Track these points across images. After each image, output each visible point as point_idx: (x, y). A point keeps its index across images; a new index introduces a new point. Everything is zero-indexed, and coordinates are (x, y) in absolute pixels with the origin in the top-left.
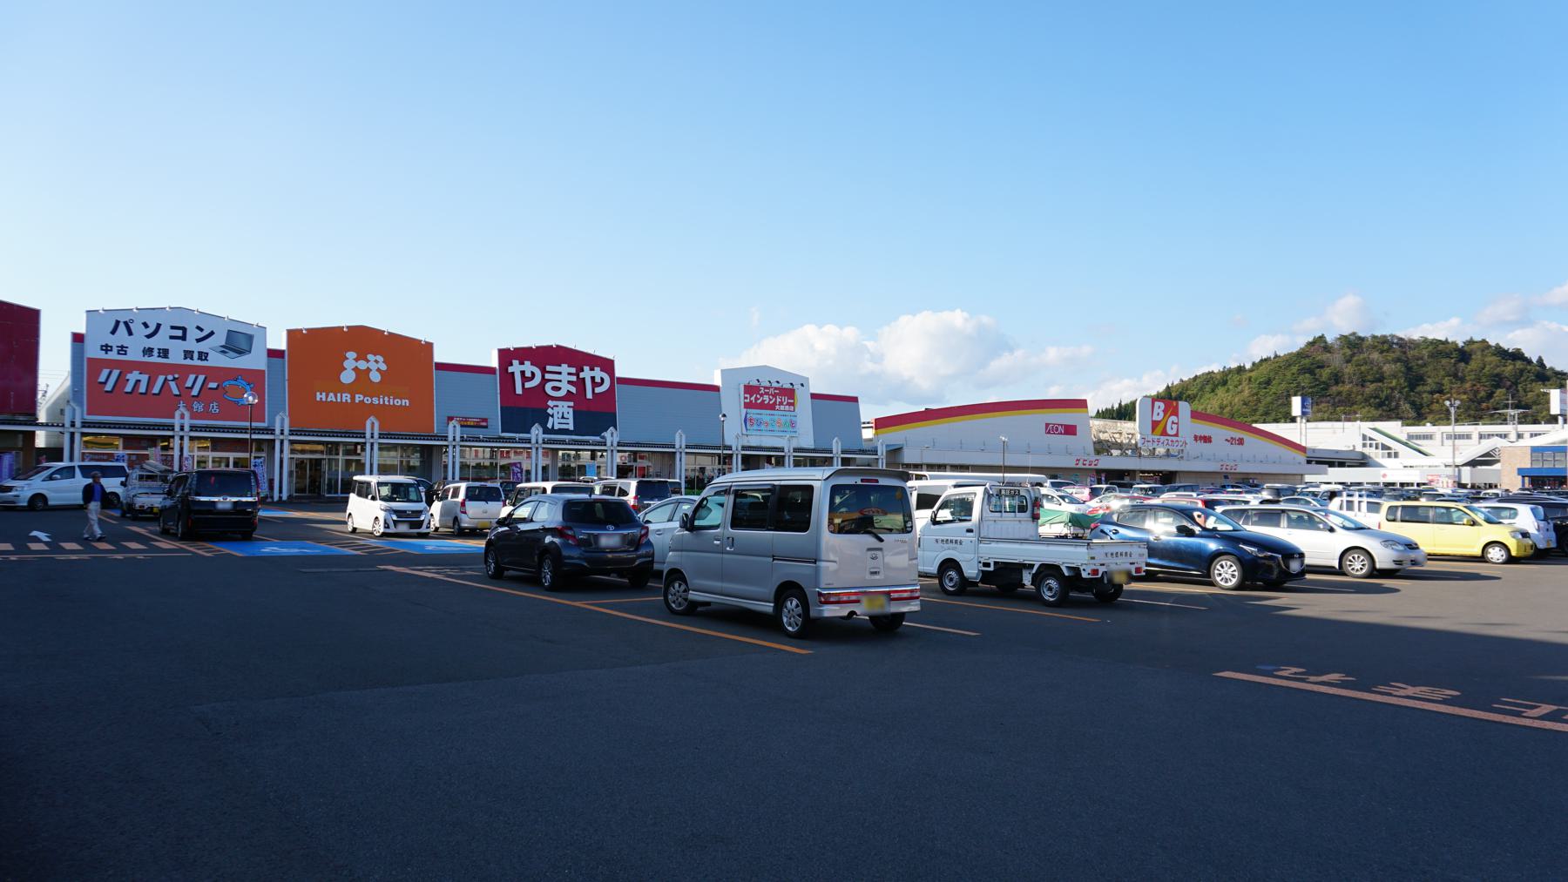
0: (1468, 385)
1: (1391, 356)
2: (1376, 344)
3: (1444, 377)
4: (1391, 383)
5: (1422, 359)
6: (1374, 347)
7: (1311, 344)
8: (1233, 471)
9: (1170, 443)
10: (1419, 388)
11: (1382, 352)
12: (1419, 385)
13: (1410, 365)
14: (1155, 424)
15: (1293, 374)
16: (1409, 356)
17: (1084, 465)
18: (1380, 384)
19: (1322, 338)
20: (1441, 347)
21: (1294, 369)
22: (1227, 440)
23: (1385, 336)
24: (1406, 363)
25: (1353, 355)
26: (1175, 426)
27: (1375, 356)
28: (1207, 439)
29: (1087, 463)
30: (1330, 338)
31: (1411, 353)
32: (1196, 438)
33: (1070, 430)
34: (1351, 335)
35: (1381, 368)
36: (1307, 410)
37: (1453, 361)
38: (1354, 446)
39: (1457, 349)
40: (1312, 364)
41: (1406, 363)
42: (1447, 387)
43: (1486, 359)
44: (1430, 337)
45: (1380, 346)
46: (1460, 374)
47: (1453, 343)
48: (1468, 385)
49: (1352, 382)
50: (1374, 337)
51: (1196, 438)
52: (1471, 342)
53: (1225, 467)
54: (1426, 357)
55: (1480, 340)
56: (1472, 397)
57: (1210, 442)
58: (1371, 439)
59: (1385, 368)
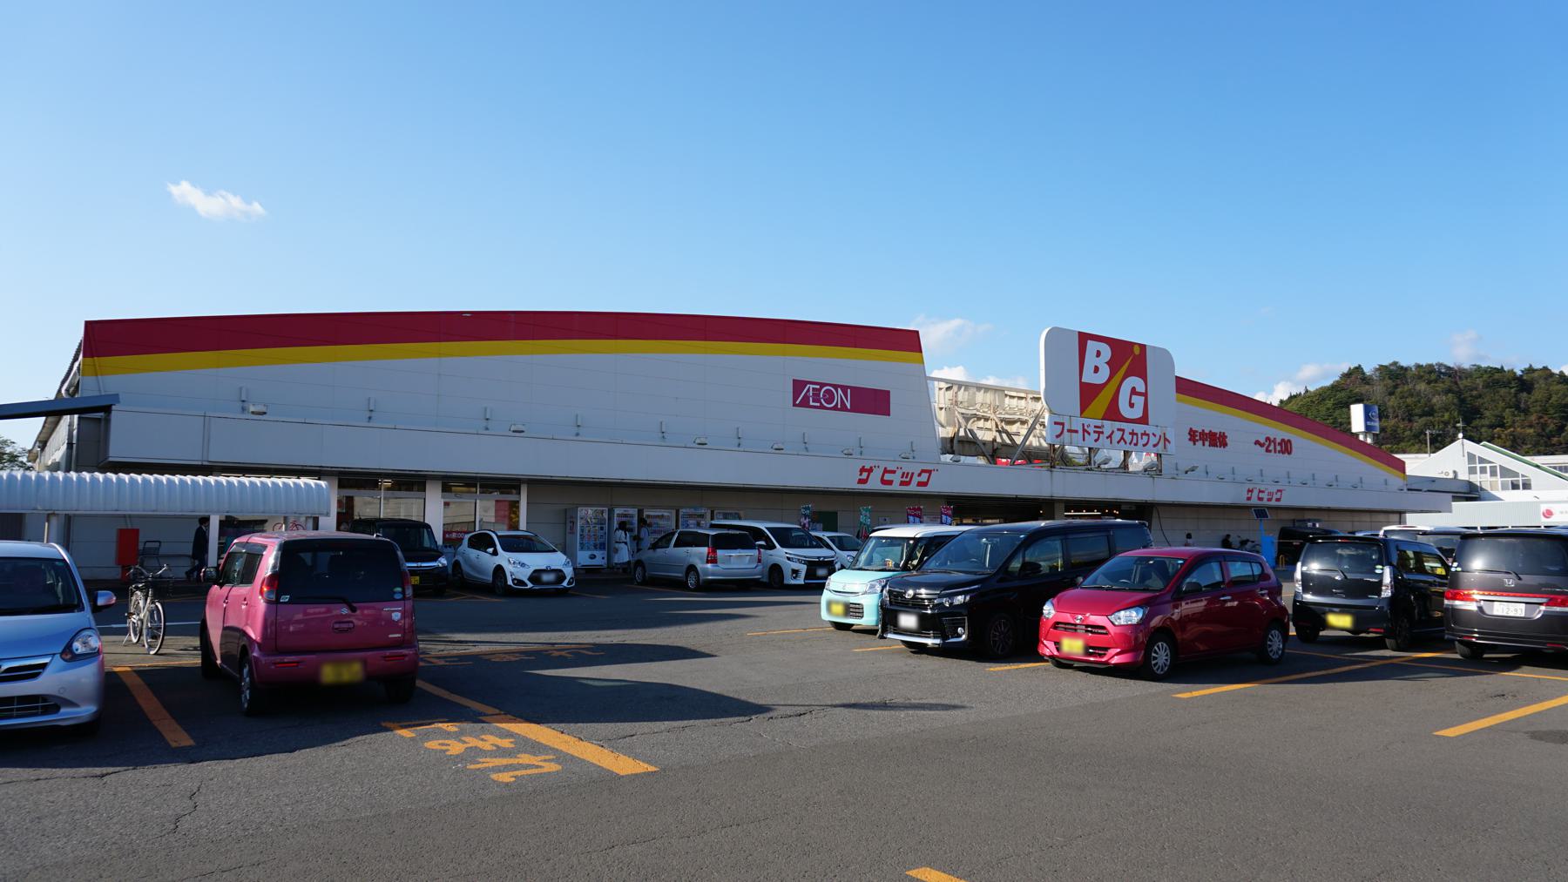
0: (1533, 418)
1: (1440, 387)
2: (1422, 374)
3: (1504, 409)
4: (1443, 416)
5: (1476, 389)
6: (1420, 377)
7: (1347, 376)
8: (1273, 503)
9: (1128, 437)
10: (1476, 423)
11: (1429, 383)
12: (1475, 419)
13: (1463, 396)
14: (1088, 393)
15: (1328, 409)
16: (1461, 386)
17: (884, 482)
18: (1431, 418)
19: (1359, 369)
20: (1497, 376)
21: (1330, 403)
22: (1257, 442)
23: (1431, 366)
24: (1459, 394)
25: (1396, 387)
26: (1139, 401)
27: (1422, 386)
28: (1217, 440)
29: (896, 478)
30: (1368, 369)
31: (1463, 383)
32: (1193, 435)
33: (873, 402)
34: (1391, 365)
35: (1429, 400)
36: (1372, 424)
37: (1513, 390)
38: (1455, 472)
39: (1520, 379)
40: (1350, 397)
41: (1459, 394)
42: (1508, 420)
43: (1551, 388)
44: (1484, 365)
45: (1427, 376)
46: (1522, 406)
47: (1509, 371)
48: (1533, 418)
49: (1397, 416)
50: (1418, 366)
51: (1193, 435)
52: (1530, 370)
53: (1256, 493)
54: (1481, 387)
55: (1541, 367)
56: (1540, 431)
57: (1225, 445)
58: (1482, 460)
59: (1434, 400)
